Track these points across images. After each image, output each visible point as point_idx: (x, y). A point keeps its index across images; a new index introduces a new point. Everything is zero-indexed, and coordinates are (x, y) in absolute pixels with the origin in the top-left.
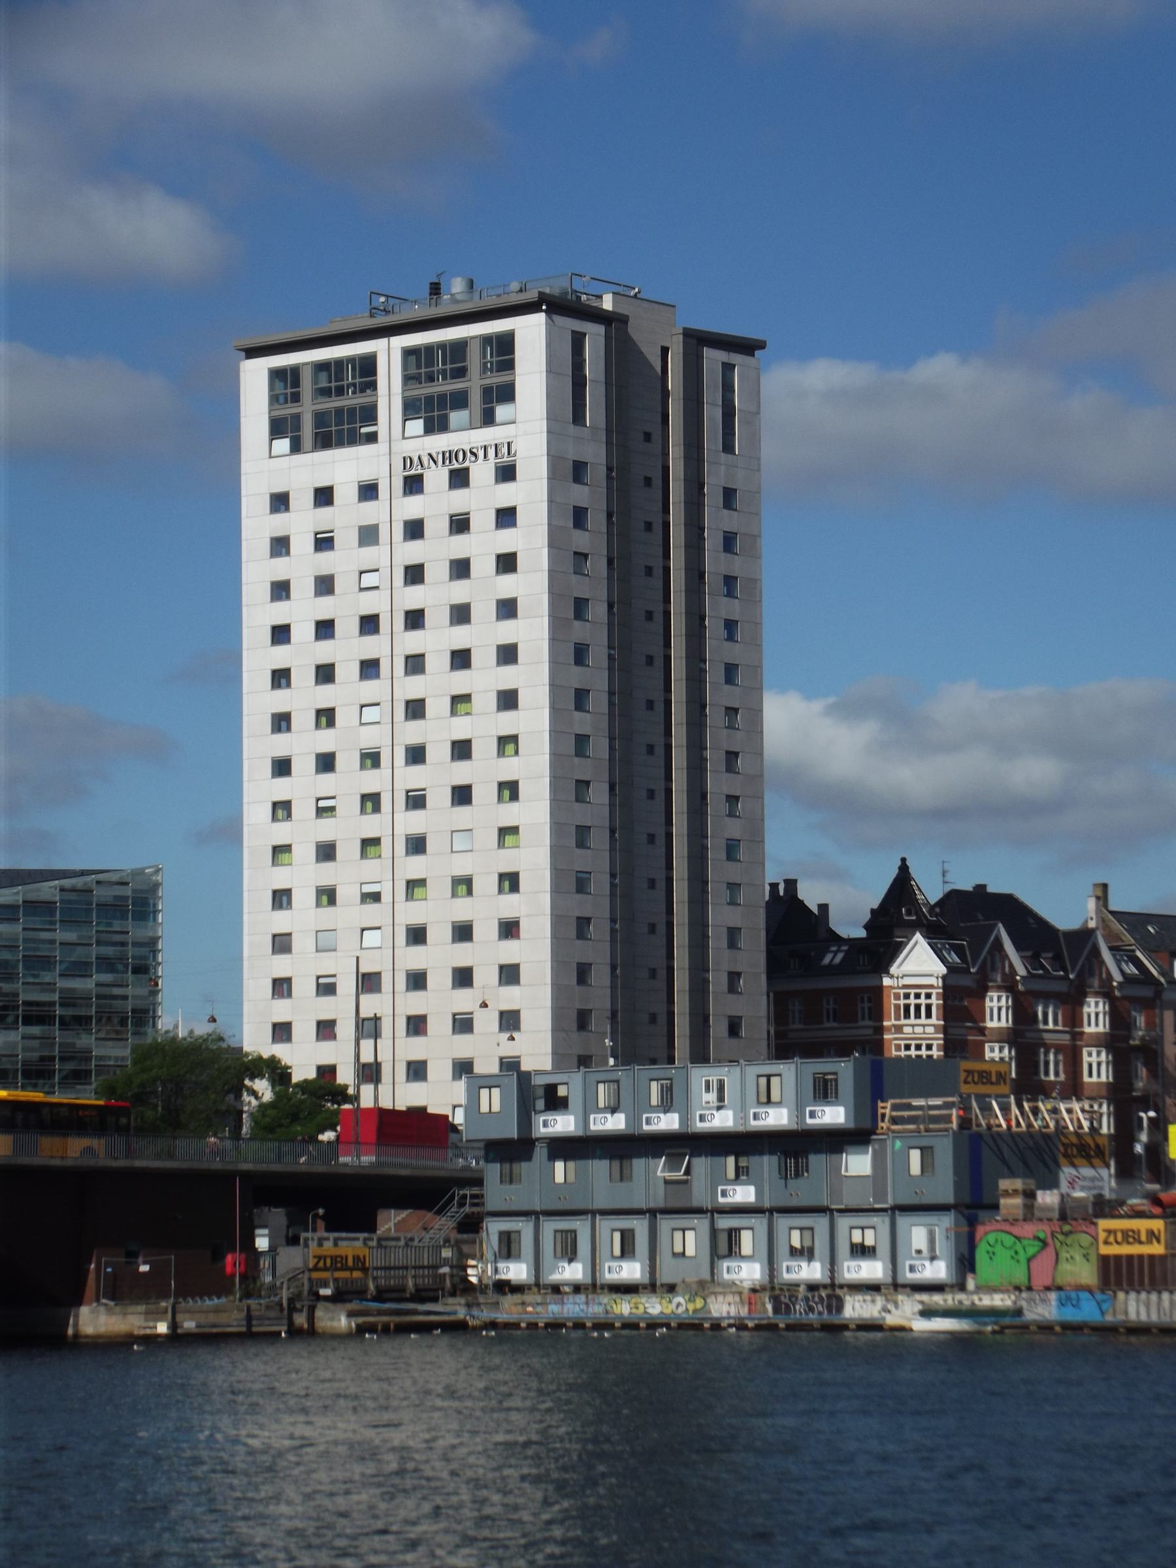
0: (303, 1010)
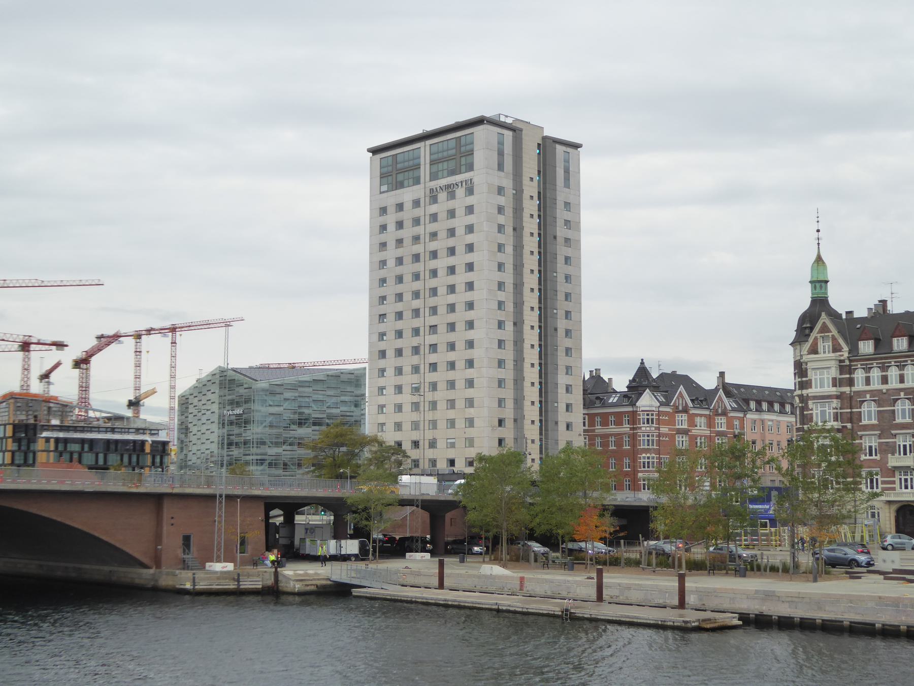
0: (390, 417)
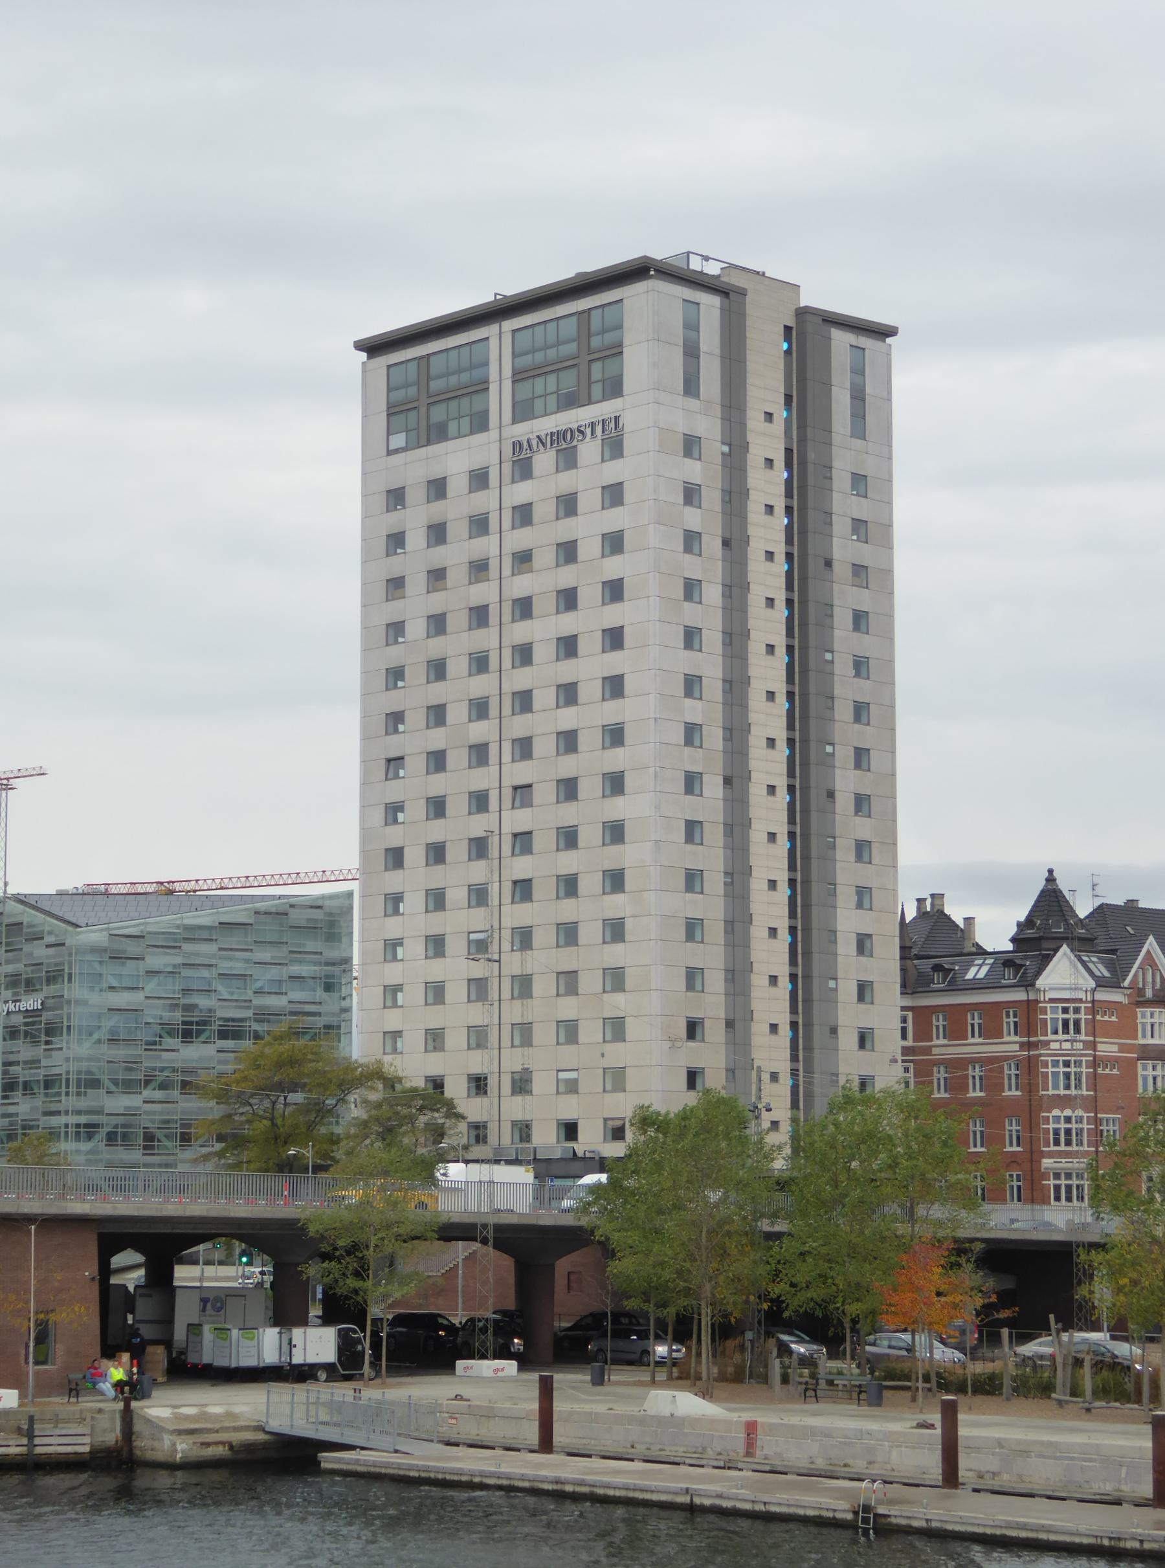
0: (414, 1018)
